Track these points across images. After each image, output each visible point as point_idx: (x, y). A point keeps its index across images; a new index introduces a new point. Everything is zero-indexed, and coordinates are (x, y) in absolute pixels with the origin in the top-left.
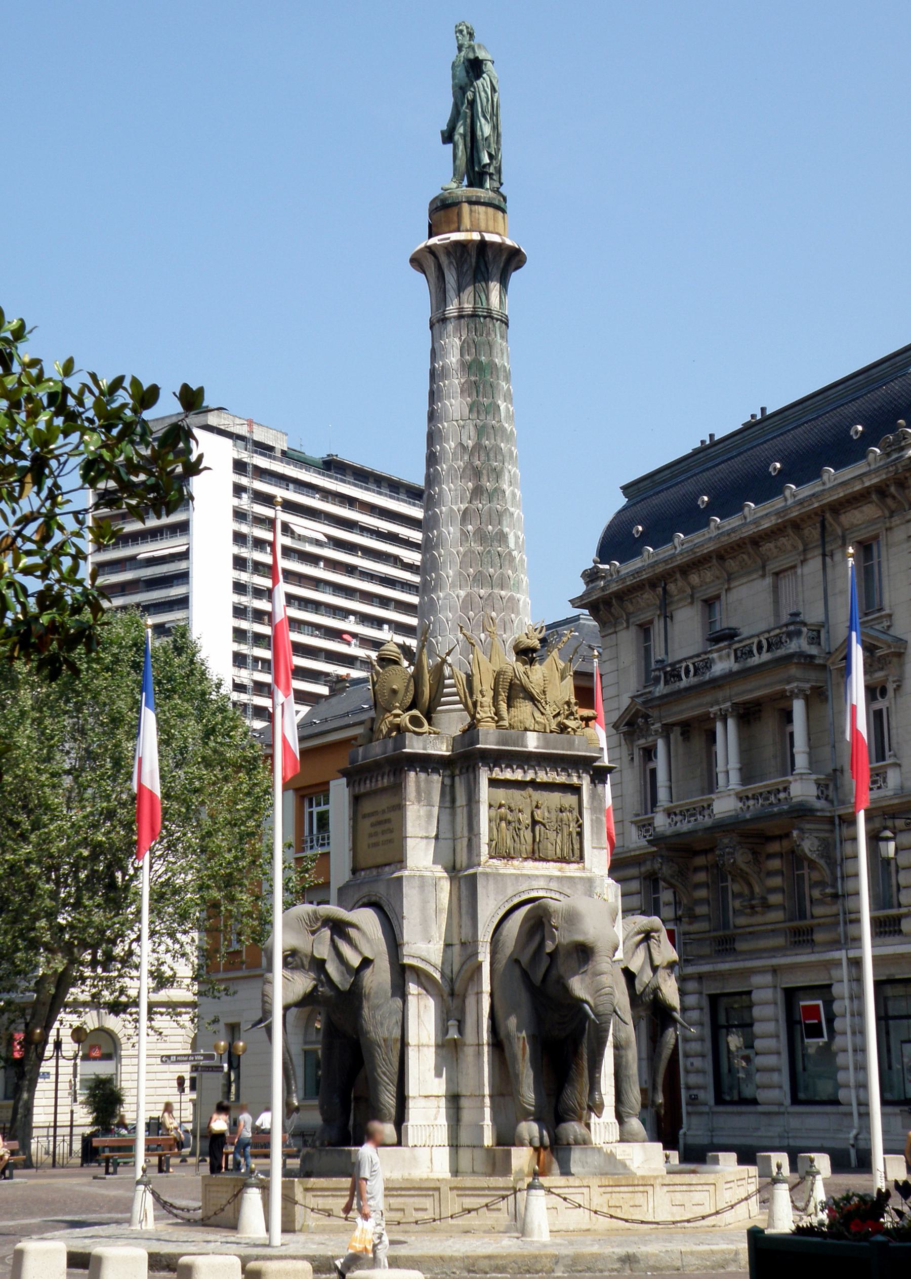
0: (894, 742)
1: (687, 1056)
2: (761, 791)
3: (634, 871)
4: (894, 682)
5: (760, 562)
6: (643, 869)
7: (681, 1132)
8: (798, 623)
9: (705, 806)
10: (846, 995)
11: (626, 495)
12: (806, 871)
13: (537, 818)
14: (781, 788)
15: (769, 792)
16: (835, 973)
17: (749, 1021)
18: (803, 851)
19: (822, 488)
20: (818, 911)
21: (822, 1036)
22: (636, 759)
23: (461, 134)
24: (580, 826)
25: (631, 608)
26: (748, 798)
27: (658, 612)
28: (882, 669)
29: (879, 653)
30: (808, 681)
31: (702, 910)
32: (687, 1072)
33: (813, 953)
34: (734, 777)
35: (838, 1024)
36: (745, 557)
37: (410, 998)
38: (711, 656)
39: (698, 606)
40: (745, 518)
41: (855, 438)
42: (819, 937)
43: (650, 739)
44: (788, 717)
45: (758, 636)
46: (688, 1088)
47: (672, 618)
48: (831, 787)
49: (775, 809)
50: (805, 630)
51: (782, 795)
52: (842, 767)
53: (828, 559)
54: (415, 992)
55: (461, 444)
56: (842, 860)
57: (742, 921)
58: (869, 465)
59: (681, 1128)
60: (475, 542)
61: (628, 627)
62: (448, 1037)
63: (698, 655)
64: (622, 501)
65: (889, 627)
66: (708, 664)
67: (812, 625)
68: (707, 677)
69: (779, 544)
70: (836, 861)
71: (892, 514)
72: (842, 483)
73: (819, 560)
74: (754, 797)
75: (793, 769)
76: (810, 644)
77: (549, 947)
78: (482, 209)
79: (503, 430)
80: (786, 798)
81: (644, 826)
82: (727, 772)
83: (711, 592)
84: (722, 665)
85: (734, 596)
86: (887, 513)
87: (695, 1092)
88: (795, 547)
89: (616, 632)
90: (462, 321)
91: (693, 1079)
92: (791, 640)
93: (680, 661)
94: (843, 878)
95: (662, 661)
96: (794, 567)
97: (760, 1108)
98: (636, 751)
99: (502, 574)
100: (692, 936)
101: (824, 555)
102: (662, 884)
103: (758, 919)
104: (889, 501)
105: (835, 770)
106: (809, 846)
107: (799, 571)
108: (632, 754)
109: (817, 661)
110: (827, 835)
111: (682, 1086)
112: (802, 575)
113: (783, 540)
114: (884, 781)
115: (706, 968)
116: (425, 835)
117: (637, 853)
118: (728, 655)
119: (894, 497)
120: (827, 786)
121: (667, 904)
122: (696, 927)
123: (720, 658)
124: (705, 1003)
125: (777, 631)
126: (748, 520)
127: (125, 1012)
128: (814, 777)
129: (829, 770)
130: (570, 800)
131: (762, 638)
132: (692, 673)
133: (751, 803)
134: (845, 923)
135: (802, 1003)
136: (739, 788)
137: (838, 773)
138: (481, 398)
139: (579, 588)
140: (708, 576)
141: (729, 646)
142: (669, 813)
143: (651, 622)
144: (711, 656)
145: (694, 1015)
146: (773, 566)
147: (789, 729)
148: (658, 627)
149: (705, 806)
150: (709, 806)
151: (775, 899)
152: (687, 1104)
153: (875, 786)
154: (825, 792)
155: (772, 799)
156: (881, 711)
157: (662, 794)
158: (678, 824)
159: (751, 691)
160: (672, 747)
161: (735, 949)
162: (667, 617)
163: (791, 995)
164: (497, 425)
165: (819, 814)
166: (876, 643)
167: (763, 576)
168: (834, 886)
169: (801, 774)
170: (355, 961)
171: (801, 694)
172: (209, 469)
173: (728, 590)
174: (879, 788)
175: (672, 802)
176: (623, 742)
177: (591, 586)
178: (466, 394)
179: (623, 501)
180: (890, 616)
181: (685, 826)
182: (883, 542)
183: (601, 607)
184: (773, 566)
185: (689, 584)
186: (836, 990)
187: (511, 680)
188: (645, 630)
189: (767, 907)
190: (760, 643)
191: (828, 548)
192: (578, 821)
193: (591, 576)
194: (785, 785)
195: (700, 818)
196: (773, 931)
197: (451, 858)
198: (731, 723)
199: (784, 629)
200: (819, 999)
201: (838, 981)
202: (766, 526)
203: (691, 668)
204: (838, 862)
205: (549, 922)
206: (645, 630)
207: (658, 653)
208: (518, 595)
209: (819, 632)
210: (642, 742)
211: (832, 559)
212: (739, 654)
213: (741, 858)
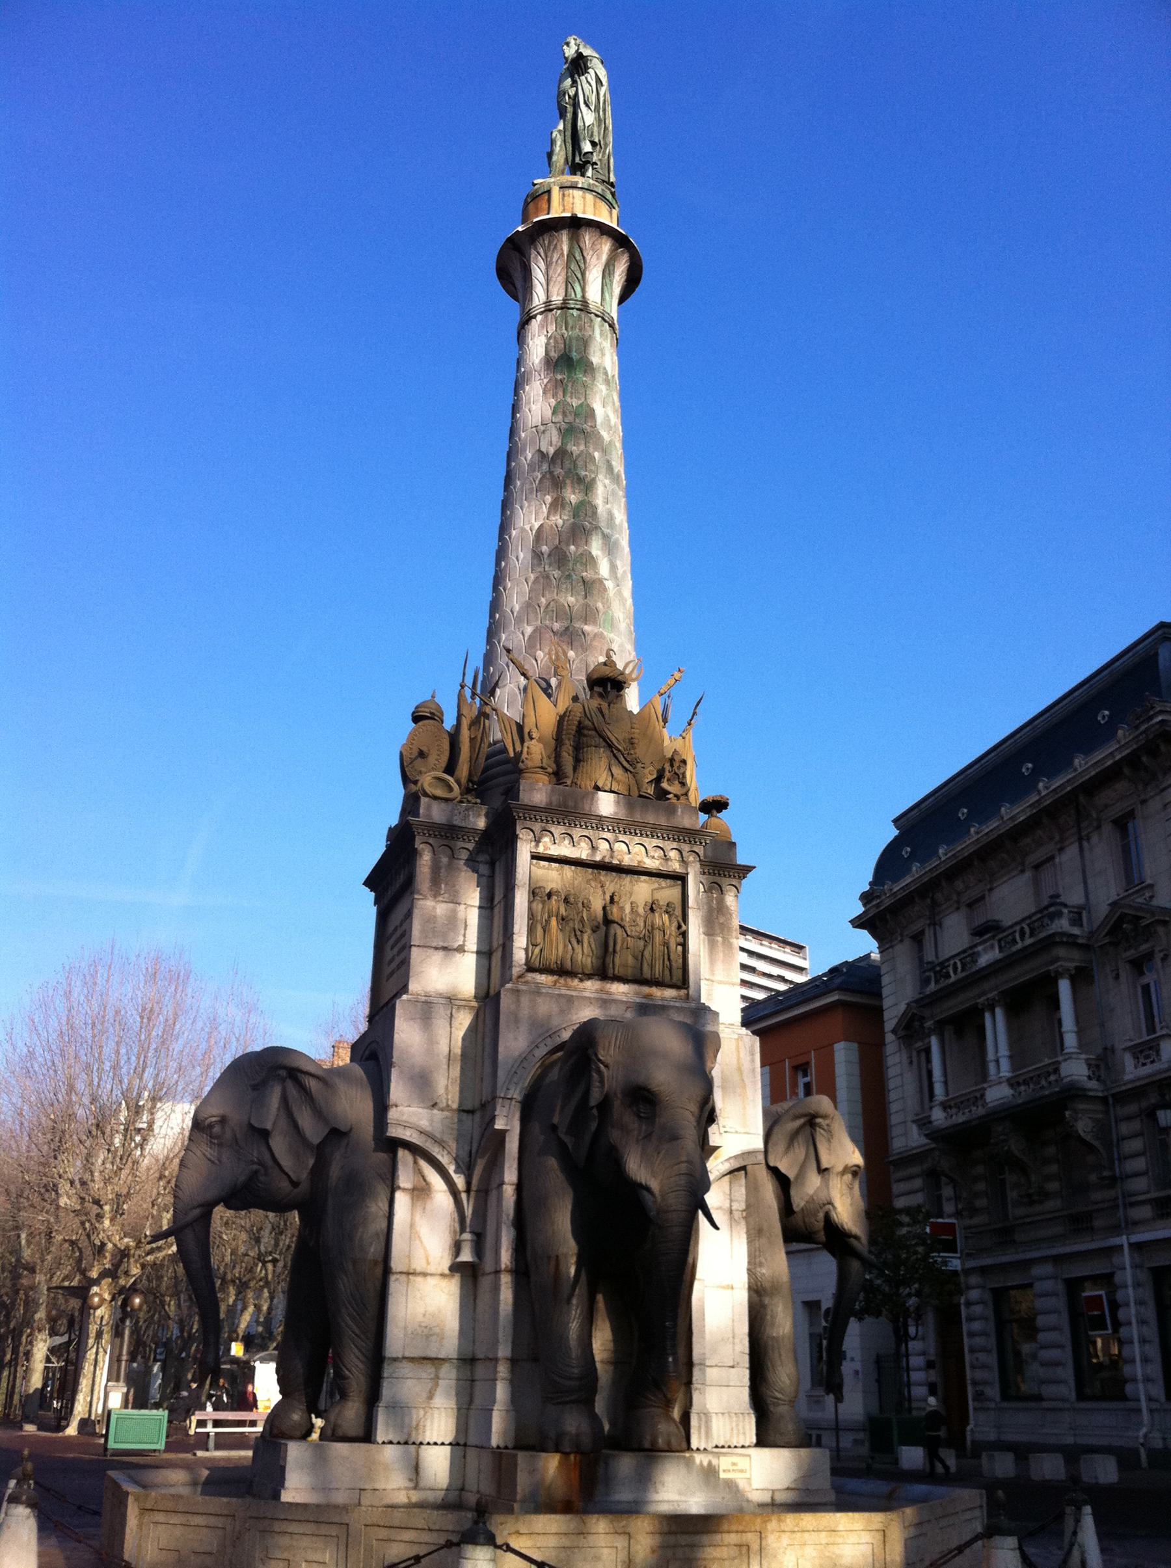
2: (1031, 1075)
3: (916, 1169)
4: (1160, 951)
6: (925, 1166)
7: (969, 1428)
9: (978, 1096)
10: (1129, 1281)
11: (897, 828)
13: (610, 917)
15: (1039, 1076)
16: (1116, 1260)
19: (1074, 774)
21: (1106, 1329)
23: (560, 131)
24: (684, 935)
26: (1019, 1084)
28: (1147, 941)
29: (1144, 923)
30: (1072, 960)
31: (981, 1203)
32: (973, 1367)
33: (1093, 1240)
34: (1005, 1064)
36: (1005, 856)
37: (399, 1195)
38: (976, 950)
41: (1102, 722)
44: (1054, 1003)
46: (975, 1383)
47: (941, 926)
48: (1102, 1067)
49: (1047, 1093)
50: (1065, 911)
51: (1052, 1078)
52: (1113, 1046)
53: (1085, 844)
54: (408, 1185)
55: (539, 451)
56: (1118, 1140)
58: (1118, 742)
59: (968, 1424)
60: (550, 565)
62: (460, 1259)
63: (964, 951)
64: (893, 832)
66: (974, 957)
67: (1073, 907)
72: (1096, 763)
73: (1076, 845)
74: (1026, 1083)
75: (1062, 1050)
76: (1071, 925)
77: (596, 1097)
78: (577, 193)
79: (599, 437)
80: (1056, 1081)
81: (924, 1124)
82: (997, 1061)
87: (981, 1388)
89: (892, 947)
90: (550, 315)
91: (980, 1375)
92: (1052, 922)
93: (948, 960)
96: (1052, 858)
97: (1045, 1404)
98: (914, 1054)
99: (587, 605)
101: (1080, 839)
102: (944, 1179)
105: (1105, 1049)
106: (1083, 1127)
107: (1057, 860)
108: (911, 1057)
109: (1080, 941)
110: (1100, 1116)
111: (969, 1382)
112: (1060, 864)
115: (988, 1261)
116: (441, 944)
117: (918, 1150)
118: (992, 947)
120: (1098, 1066)
122: (976, 1221)
123: (985, 950)
124: (988, 1297)
125: (1039, 915)
126: (1005, 819)
128: (1083, 1056)
129: (1099, 1050)
130: (671, 893)
131: (1024, 925)
133: (1022, 1088)
134: (1125, 1205)
135: (1084, 1294)
136: (1008, 1075)
138: (569, 400)
139: (859, 909)
141: (993, 937)
142: (945, 1106)
143: (922, 933)
144: (976, 950)
148: (929, 934)
149: (978, 1096)
150: (983, 1096)
152: (974, 1400)
153: (1149, 1061)
154: (1097, 1073)
155: (1043, 1082)
156: (1148, 985)
157: (939, 1089)
158: (954, 1117)
162: (935, 924)
163: (1073, 1286)
164: (589, 429)
165: (1091, 1094)
166: (1139, 914)
167: (1023, 871)
168: (1112, 1168)
173: (991, 890)
174: (1152, 1062)
177: (868, 906)
178: (550, 395)
180: (1151, 886)
181: (961, 1118)
186: (1118, 1279)
187: (580, 722)
188: (918, 939)
189: (1045, 1195)
190: (1022, 929)
191: (1084, 833)
192: (679, 927)
193: (866, 898)
196: (1051, 1219)
197: (486, 984)
198: (999, 1012)
200: (1101, 1289)
201: (1121, 1269)
202: (1022, 819)
204: (1115, 1143)
205: (596, 1055)
206: (918, 939)
207: (930, 956)
208: (612, 635)
209: (1080, 914)
210: (919, 1044)
211: (1089, 843)
212: (1003, 944)
213: (1015, 1146)
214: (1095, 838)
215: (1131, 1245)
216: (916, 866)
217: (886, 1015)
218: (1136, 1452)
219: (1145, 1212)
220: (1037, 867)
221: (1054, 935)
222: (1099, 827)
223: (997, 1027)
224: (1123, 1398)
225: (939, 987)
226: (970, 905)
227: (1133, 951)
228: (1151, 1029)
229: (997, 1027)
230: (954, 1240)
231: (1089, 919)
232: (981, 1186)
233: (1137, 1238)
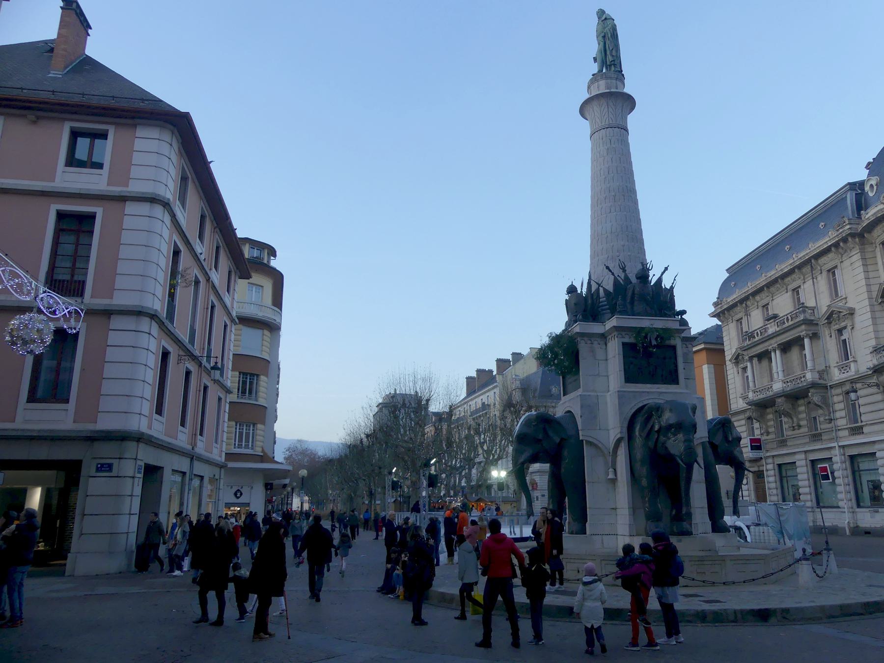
0: (853, 351)
1: (770, 495)
4: (850, 326)
5: (785, 287)
6: (746, 416)
8: (804, 307)
14: (802, 376)
17: (796, 474)
20: (823, 426)
22: (740, 372)
25: (733, 314)
27: (744, 314)
30: (810, 330)
34: (781, 374)
35: (836, 474)
36: (778, 286)
40: (777, 270)
42: (824, 437)
43: (745, 364)
45: (786, 315)
49: (800, 385)
57: (823, 426)
61: (732, 322)
63: (762, 327)
65: (846, 303)
66: (766, 330)
68: (766, 335)
69: (792, 278)
70: (829, 405)
71: (842, 255)
75: (807, 368)
84: (772, 329)
85: (775, 302)
93: (755, 330)
94: (833, 412)
95: (747, 332)
100: (768, 441)
101: (813, 278)
103: (797, 432)
114: (850, 369)
121: (757, 429)
123: (771, 327)
131: (788, 316)
132: (759, 335)
135: (819, 466)
137: (828, 368)
145: (775, 492)
147: (804, 353)
148: (744, 321)
151: (803, 423)
160: (754, 368)
161: (787, 445)
162: (747, 314)
167: (787, 292)
169: (811, 369)
171: (807, 335)
174: (847, 372)
175: (755, 387)
176: (734, 366)
179: (728, 275)
183: (721, 315)
185: (756, 301)
188: (739, 321)
194: (804, 375)
195: (768, 392)
198: (778, 352)
199: (798, 311)
203: (759, 333)
214: (819, 278)
217: (726, 354)
219: (846, 433)
222: (821, 273)
225: (750, 342)
232: (772, 423)
233: (841, 444)
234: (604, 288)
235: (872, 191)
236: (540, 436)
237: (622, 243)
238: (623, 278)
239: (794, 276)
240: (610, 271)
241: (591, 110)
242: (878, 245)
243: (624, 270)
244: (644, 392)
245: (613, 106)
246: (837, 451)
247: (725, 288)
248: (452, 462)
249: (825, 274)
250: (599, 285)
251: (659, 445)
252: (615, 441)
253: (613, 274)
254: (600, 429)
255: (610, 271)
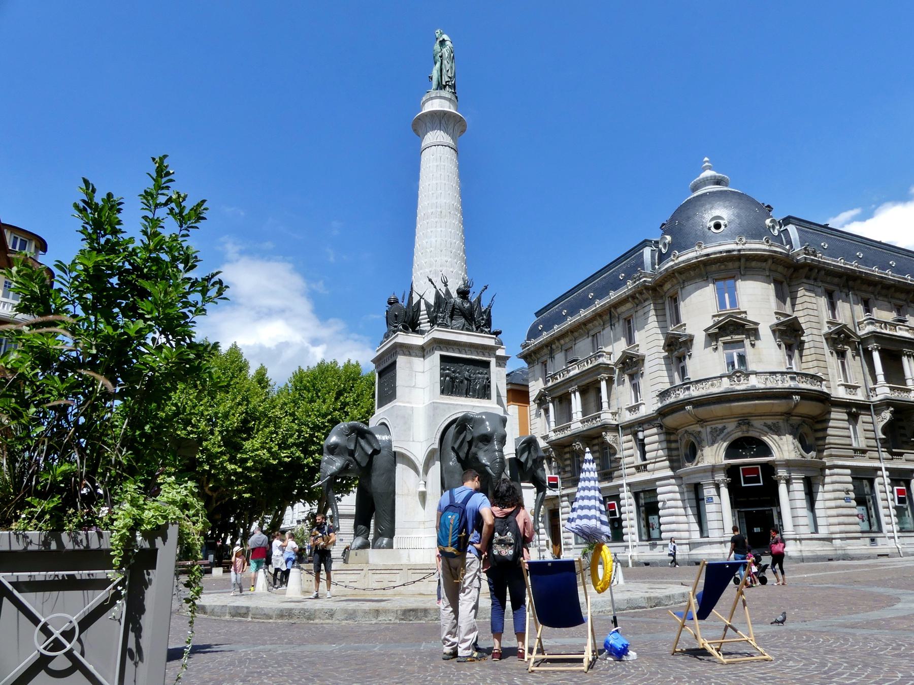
12: (608, 450)
18: (606, 441)
26: (584, 422)
31: (568, 469)
39: (563, 352)
51: (598, 419)
53: (613, 327)
71: (637, 305)
83: (569, 346)
86: (635, 306)
88: (600, 324)
101: (611, 325)
104: (636, 300)
107: (602, 333)
113: (595, 322)
119: (637, 298)
122: (566, 476)
127: (150, 280)
140: (567, 340)
143: (546, 361)
146: (592, 333)
148: (549, 361)
159: (585, 380)
167: (588, 337)
170: (370, 451)
172: (198, 228)
173: (575, 344)
180: (685, 325)
182: (634, 317)
184: (592, 333)
188: (544, 364)
195: (566, 432)
198: (578, 394)
214: (617, 325)
215: (626, 484)
216: (569, 318)
217: (530, 394)
218: (627, 562)
220: (566, 350)
221: (600, 364)
222: (619, 321)
223: (576, 402)
224: (623, 541)
225: (553, 384)
226: (566, 350)
227: (630, 370)
228: (637, 400)
229: (576, 402)
230: (557, 483)
231: (614, 357)
232: (568, 462)
234: (425, 301)
235: (665, 248)
236: (352, 447)
237: (446, 259)
238: (444, 292)
239: (596, 322)
240: (432, 283)
241: (424, 126)
242: (667, 298)
243: (446, 285)
244: (457, 405)
245: (445, 126)
246: (625, 488)
247: (533, 333)
248: (224, 540)
249: (621, 322)
250: (421, 297)
251: (470, 456)
252: (428, 451)
253: (435, 287)
254: (413, 441)
255: (432, 283)
